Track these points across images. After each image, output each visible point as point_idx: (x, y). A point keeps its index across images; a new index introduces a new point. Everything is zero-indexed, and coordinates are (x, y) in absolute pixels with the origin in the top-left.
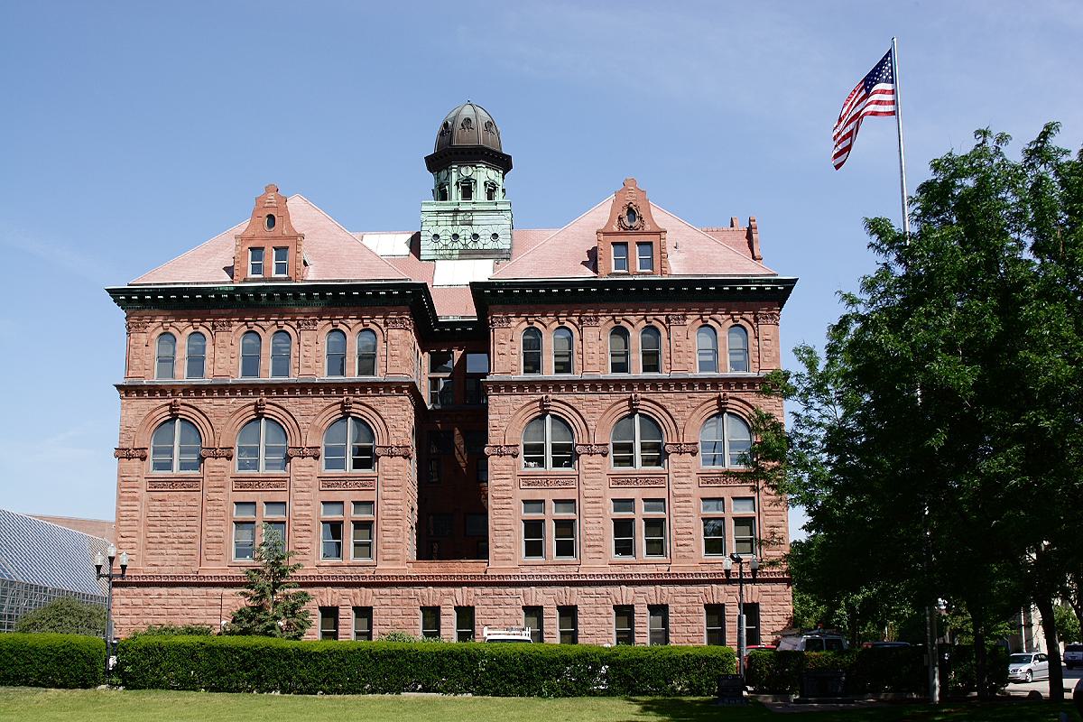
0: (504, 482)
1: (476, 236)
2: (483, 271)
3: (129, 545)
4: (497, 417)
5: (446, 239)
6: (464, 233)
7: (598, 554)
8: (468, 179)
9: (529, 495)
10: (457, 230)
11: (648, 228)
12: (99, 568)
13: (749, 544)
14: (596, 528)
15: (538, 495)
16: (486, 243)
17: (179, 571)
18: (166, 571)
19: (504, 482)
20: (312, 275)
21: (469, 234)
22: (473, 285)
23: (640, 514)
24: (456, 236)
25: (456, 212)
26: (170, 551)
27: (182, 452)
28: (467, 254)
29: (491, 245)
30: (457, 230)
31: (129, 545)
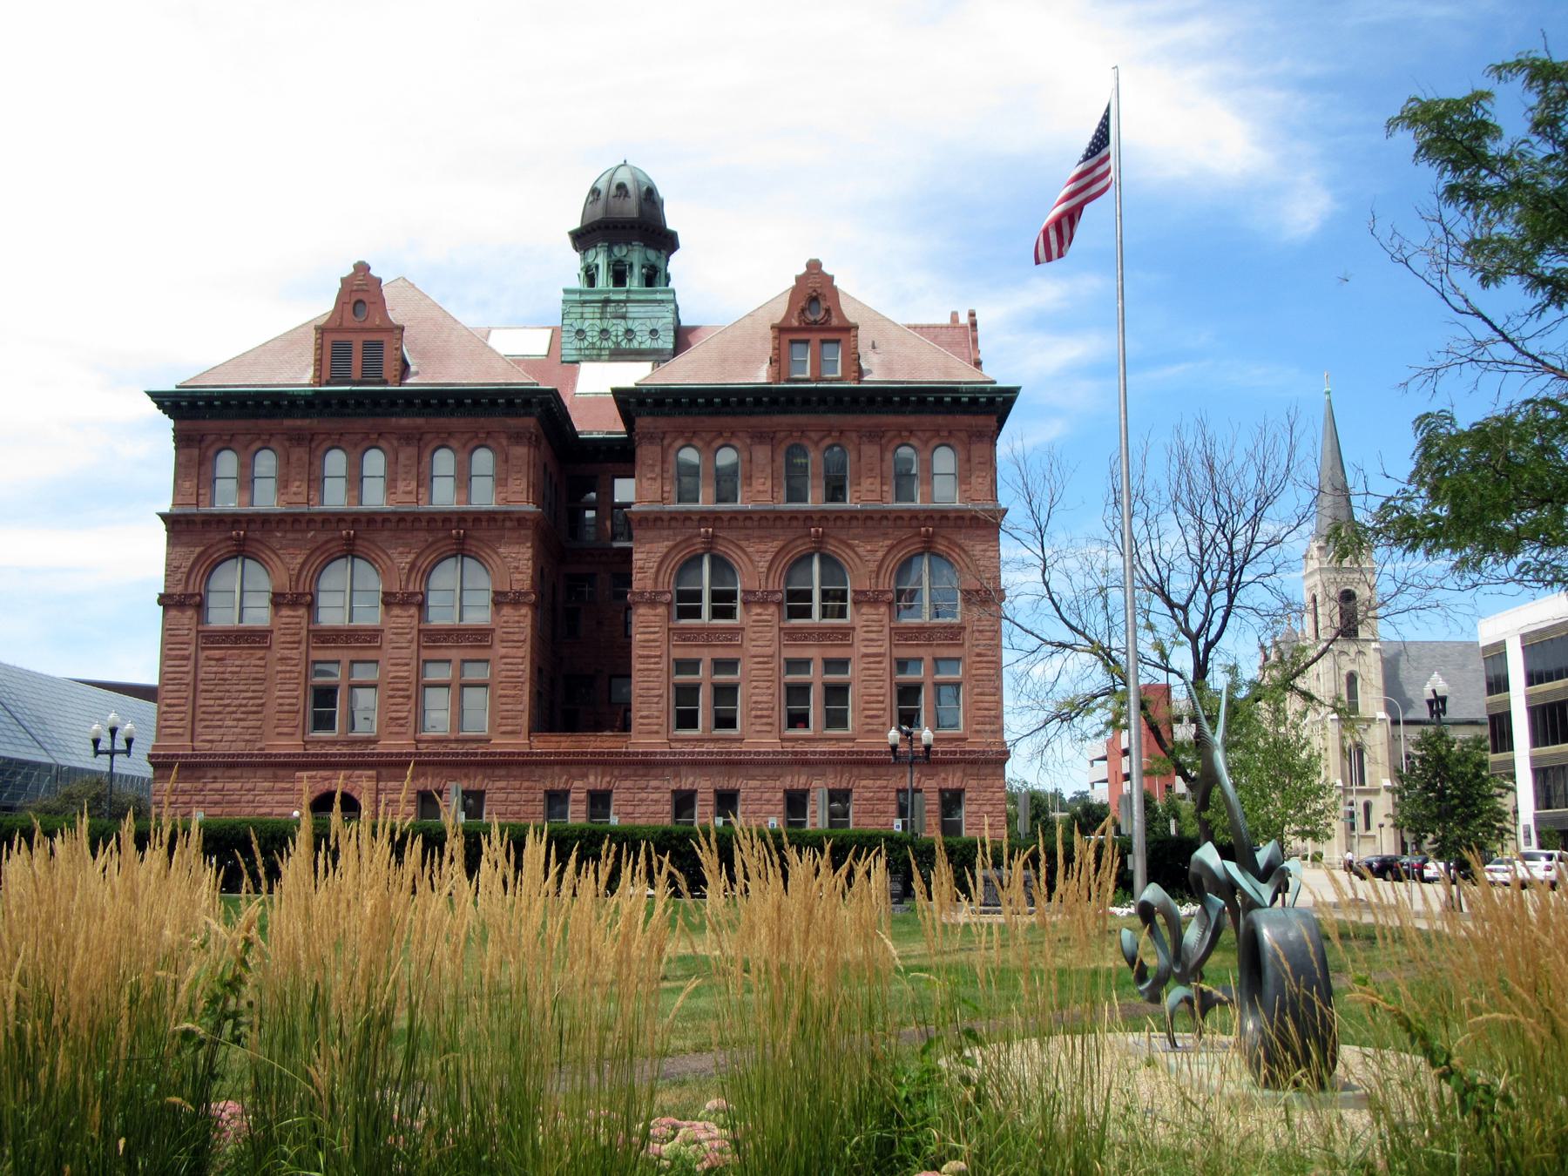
0: (652, 637)
1: (629, 331)
2: (632, 375)
3: (178, 716)
4: (643, 556)
5: (592, 336)
6: (617, 328)
7: (757, 731)
8: (619, 262)
9: (678, 653)
10: (606, 324)
11: (835, 322)
12: (96, 742)
13: (358, 691)
14: (758, 692)
15: (693, 654)
16: (643, 341)
17: (238, 747)
18: (221, 748)
19: (652, 637)
20: (413, 382)
21: (621, 330)
22: (616, 392)
23: (816, 677)
24: (604, 332)
25: (606, 302)
26: (230, 723)
27: (1532, 678)
28: (618, 355)
29: (648, 344)
30: (606, 324)
31: (178, 716)
